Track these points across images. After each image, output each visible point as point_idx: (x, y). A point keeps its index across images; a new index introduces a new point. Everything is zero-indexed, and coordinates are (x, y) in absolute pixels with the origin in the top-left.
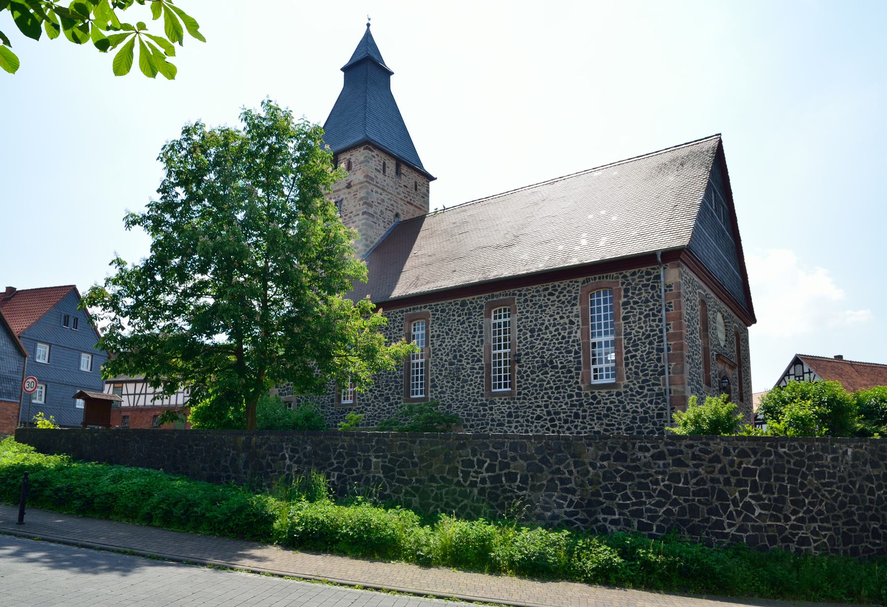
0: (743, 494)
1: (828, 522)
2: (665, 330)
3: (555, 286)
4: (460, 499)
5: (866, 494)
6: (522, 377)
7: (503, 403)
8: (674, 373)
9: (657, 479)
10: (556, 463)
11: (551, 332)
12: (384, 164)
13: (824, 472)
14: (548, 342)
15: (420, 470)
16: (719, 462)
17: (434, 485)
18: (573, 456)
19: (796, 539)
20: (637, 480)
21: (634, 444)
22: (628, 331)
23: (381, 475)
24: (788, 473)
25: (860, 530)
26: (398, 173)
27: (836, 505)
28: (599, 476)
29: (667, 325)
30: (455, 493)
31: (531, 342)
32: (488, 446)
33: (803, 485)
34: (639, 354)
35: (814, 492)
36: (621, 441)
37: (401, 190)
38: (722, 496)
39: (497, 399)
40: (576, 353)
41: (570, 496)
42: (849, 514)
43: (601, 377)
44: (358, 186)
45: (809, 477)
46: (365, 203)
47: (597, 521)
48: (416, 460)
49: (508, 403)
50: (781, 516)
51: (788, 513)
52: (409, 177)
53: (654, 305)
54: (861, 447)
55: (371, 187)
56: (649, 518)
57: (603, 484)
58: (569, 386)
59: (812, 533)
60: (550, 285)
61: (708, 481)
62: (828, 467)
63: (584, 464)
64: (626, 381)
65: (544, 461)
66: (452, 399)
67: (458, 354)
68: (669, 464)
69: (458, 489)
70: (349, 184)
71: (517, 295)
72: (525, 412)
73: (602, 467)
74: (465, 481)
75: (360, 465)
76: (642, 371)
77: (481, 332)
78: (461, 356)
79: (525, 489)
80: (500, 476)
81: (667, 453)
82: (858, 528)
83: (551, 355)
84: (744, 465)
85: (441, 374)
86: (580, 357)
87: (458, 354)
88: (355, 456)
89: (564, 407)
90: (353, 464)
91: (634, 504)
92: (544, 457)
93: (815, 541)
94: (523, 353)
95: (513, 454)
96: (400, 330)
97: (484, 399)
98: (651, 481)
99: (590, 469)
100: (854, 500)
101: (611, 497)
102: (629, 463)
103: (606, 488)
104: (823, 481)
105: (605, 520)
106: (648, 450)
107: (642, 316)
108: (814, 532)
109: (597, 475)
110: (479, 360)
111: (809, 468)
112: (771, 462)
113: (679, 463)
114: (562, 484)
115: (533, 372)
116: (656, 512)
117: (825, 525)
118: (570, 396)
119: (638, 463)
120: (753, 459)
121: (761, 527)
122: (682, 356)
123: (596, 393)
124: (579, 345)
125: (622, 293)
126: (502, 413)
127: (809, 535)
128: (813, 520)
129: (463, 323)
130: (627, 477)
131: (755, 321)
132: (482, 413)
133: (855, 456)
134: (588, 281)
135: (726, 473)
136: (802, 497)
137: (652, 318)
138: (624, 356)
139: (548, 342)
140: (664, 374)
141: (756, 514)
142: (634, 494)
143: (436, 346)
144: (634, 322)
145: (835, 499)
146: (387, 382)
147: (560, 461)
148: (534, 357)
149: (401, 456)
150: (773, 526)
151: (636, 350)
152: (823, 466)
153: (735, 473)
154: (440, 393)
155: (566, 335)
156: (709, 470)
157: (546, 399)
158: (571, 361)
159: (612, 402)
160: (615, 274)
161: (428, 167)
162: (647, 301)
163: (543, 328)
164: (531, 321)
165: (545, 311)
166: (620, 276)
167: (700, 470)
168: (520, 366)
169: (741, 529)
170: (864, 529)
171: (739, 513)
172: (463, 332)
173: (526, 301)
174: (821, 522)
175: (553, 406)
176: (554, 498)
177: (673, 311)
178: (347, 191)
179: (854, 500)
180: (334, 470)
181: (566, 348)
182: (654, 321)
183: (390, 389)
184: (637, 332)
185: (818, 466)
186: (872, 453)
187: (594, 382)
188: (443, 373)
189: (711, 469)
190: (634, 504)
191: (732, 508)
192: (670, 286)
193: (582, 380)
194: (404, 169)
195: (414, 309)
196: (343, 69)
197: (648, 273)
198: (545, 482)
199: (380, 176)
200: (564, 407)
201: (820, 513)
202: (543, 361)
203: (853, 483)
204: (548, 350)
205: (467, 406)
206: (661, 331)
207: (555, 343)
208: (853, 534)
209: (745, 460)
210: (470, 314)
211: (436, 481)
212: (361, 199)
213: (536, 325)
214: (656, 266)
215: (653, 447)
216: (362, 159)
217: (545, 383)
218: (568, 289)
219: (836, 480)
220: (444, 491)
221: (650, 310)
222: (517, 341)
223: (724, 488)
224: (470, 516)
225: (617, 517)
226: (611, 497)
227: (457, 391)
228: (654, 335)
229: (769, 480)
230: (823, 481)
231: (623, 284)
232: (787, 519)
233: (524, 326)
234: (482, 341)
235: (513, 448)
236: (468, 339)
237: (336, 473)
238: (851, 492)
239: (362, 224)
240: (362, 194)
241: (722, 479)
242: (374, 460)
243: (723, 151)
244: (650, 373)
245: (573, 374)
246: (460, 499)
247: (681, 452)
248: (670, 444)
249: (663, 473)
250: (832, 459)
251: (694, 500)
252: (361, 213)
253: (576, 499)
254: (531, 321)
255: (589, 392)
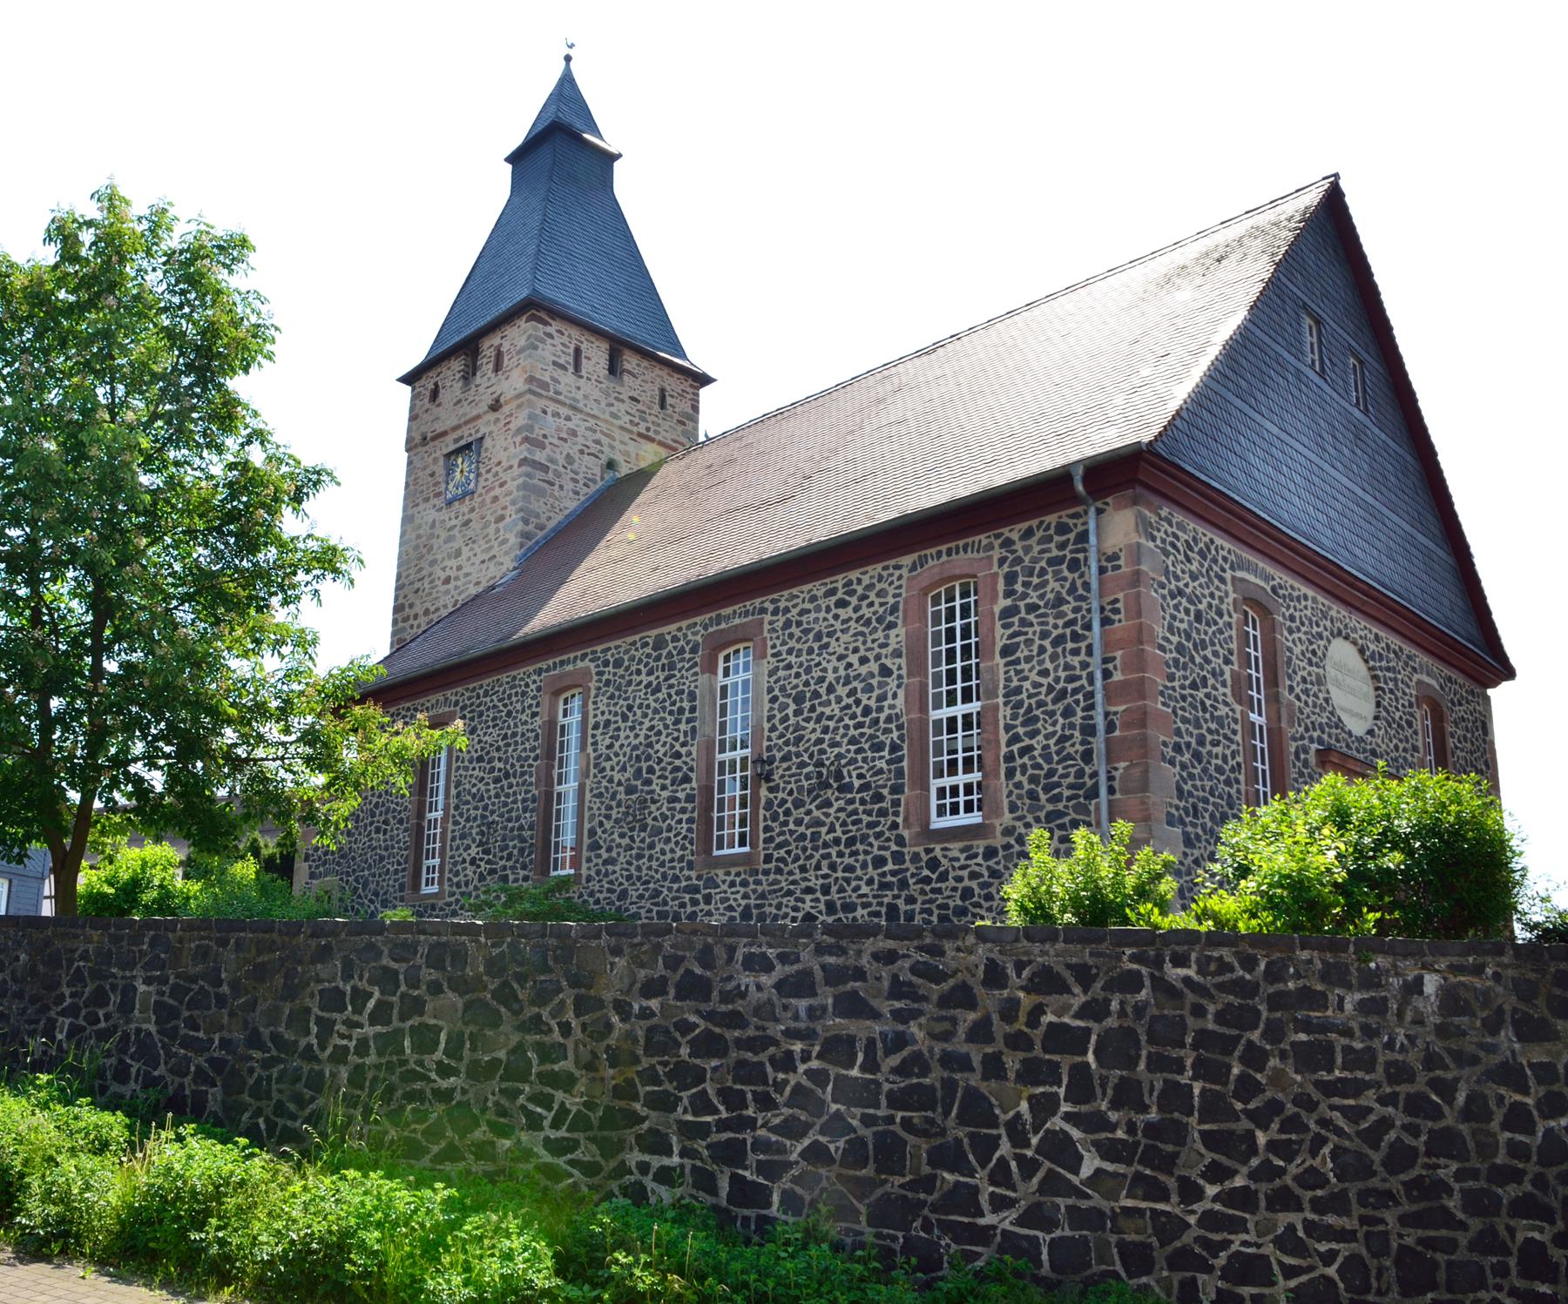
0: (1045, 1107)
1: (1344, 1211)
2: (1098, 675)
3: (850, 583)
4: (308, 1093)
5: (1495, 1125)
6: (775, 818)
7: (732, 884)
8: (1125, 791)
9: (790, 1053)
10: (533, 1003)
11: (839, 700)
12: (578, 351)
13: (1329, 1049)
14: (832, 724)
15: (231, 1015)
16: (971, 1004)
17: (257, 1055)
18: (574, 983)
19: (1222, 1259)
20: (734, 1055)
21: (732, 950)
22: (1015, 683)
23: (152, 1028)
24: (1195, 1047)
25: (1472, 1246)
26: (614, 369)
27: (1376, 1157)
28: (635, 1041)
29: (1105, 661)
30: (298, 1079)
31: (798, 728)
32: (380, 954)
33: (1247, 1088)
34: (1038, 742)
35: (1290, 1109)
36: (699, 942)
37: (620, 408)
38: (977, 1110)
39: (720, 872)
40: (895, 748)
41: (559, 1095)
42: (1429, 1189)
43: (955, 810)
44: (514, 404)
45: (1273, 1062)
46: (526, 439)
47: (623, 1169)
48: (225, 989)
49: (744, 884)
50: (1171, 1183)
51: (1194, 1174)
52: (642, 380)
53: (1076, 610)
54: (1478, 970)
55: (542, 403)
56: (762, 1168)
57: (645, 1062)
58: (878, 836)
59: (1279, 1243)
60: (840, 580)
61: (935, 1065)
62: (1347, 1032)
63: (600, 1004)
64: (1007, 818)
65: (506, 996)
66: (629, 878)
67: (644, 765)
68: (824, 1008)
69: (306, 1068)
70: (497, 401)
71: (769, 613)
72: (779, 907)
73: (646, 1014)
74: (323, 1048)
75: (115, 999)
76: (1047, 789)
77: (693, 709)
78: (651, 770)
79: (456, 1072)
80: (399, 1033)
81: (819, 974)
82: (1463, 1239)
83: (839, 756)
84: (1049, 1018)
85: (608, 817)
86: (901, 759)
87: (644, 765)
88: (106, 978)
89: (865, 890)
90: (100, 998)
91: (723, 1125)
92: (505, 984)
93: (1290, 1272)
94: (779, 755)
95: (434, 975)
96: (534, 715)
97: (693, 874)
98: (772, 1059)
99: (615, 1019)
100: (1445, 1143)
101: (664, 1103)
102: (715, 1004)
103: (651, 1077)
104: (1323, 1075)
105: (644, 1168)
106: (769, 968)
107: (1047, 643)
108: (1289, 1242)
109: (630, 1036)
110: (687, 779)
111: (1274, 1032)
112: (1140, 1010)
113: (853, 1006)
114: (542, 1061)
115: (798, 804)
116: (782, 1150)
117: (1331, 1219)
118: (879, 862)
119: (739, 1005)
120: (1079, 999)
121: (1100, 1213)
122: (1143, 742)
123: (938, 853)
124: (900, 728)
125: (1001, 586)
126: (731, 908)
127: (1269, 1250)
128: (1284, 1200)
129: (658, 690)
130: (709, 1045)
131: (1509, 673)
132: (689, 909)
133: (1451, 1000)
134: (923, 561)
135: (990, 1039)
136: (1245, 1124)
137: (1070, 645)
138: (1004, 750)
139: (832, 724)
140: (1097, 796)
141: (1086, 1171)
142: (724, 1094)
143: (602, 749)
144: (1028, 659)
145: (1373, 1136)
146: (504, 840)
147: (541, 998)
148: (802, 765)
149: (194, 979)
150: (1139, 1212)
151: (1033, 734)
152: (1325, 1027)
153: (1018, 1042)
154: (606, 862)
155: (872, 703)
156: (939, 1028)
157: (825, 871)
158: (881, 771)
159: (974, 876)
160: (983, 539)
161: (698, 356)
162: (1060, 601)
163: (823, 691)
164: (798, 675)
165: (827, 646)
166: (997, 543)
167: (913, 1028)
168: (771, 790)
169: (1035, 1216)
170: (1488, 1242)
171: (1029, 1168)
172: (656, 711)
173: (788, 624)
174: (1314, 1210)
175: (841, 890)
176: (521, 1100)
177: (1122, 623)
178: (492, 416)
179: (1445, 1143)
180: (63, 1013)
181: (872, 737)
182: (1076, 652)
183: (509, 857)
184: (1036, 685)
185: (1306, 1026)
186: (1525, 991)
187: (938, 823)
188: (614, 813)
189: (946, 1026)
190: (723, 1125)
191: (1005, 1148)
192: (1115, 557)
193: (906, 820)
194: (630, 361)
195: (562, 663)
196: (509, 159)
197: (1063, 529)
198: (502, 1055)
199: (567, 378)
200: (865, 890)
201: (1312, 1178)
202: (820, 774)
203: (1447, 1090)
204: (834, 744)
205: (657, 893)
206: (1091, 681)
207: (847, 727)
208: (1441, 1258)
209: (1054, 1000)
210: (672, 666)
211: (261, 1047)
212: (519, 431)
213: (807, 684)
214: (1080, 509)
215: (783, 958)
216: (522, 342)
217: (824, 830)
218: (879, 586)
219: (1379, 1074)
220: (275, 1072)
221: (1066, 625)
222: (767, 726)
223: (984, 1087)
224: (1329, 1241)
225: (676, 1160)
226: (664, 1103)
227: (639, 857)
228: (1075, 691)
229: (1132, 1063)
230: (1323, 1075)
231: (1002, 561)
232: (1190, 1192)
233: (783, 689)
234: (694, 729)
235: (435, 961)
236: (666, 727)
237: (68, 1021)
238: (1437, 1114)
239: (518, 488)
240: (520, 420)
241: (976, 1060)
242: (142, 988)
243: (1345, 208)
244: (1067, 793)
245: (886, 804)
246: (308, 1093)
247: (860, 974)
248: (829, 950)
249: (807, 1035)
250: (1362, 1006)
251: (890, 1120)
252: (515, 462)
253: (574, 1103)
254: (798, 675)
255: (920, 849)
